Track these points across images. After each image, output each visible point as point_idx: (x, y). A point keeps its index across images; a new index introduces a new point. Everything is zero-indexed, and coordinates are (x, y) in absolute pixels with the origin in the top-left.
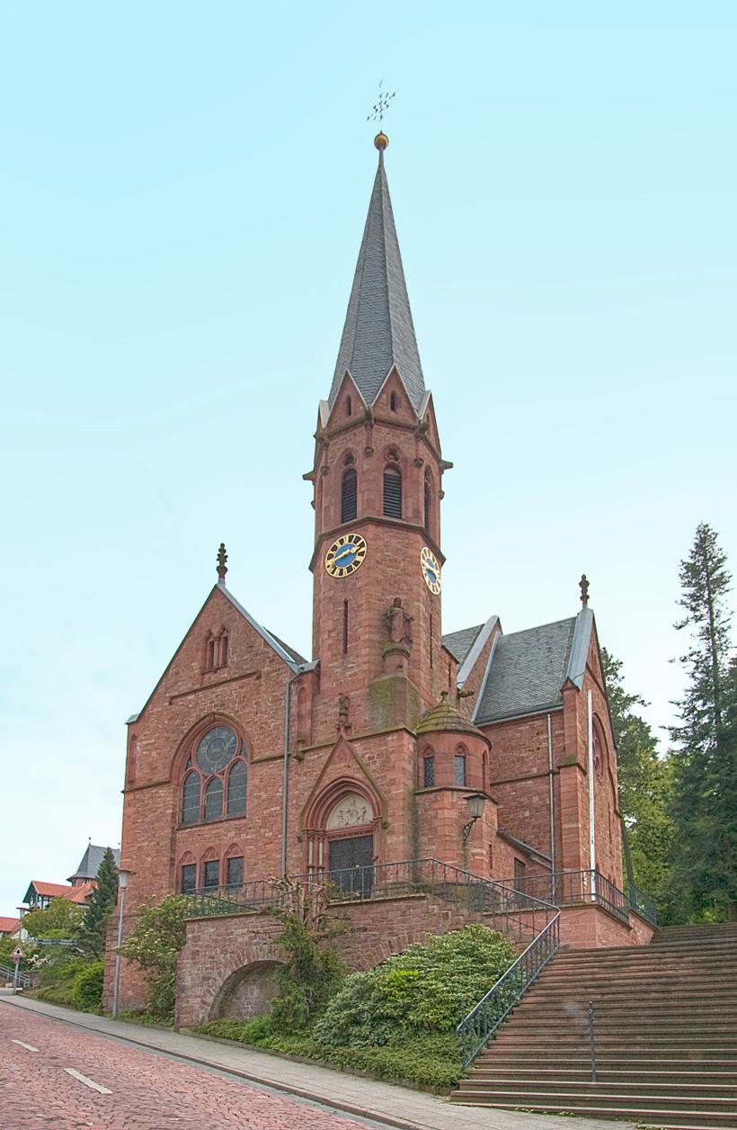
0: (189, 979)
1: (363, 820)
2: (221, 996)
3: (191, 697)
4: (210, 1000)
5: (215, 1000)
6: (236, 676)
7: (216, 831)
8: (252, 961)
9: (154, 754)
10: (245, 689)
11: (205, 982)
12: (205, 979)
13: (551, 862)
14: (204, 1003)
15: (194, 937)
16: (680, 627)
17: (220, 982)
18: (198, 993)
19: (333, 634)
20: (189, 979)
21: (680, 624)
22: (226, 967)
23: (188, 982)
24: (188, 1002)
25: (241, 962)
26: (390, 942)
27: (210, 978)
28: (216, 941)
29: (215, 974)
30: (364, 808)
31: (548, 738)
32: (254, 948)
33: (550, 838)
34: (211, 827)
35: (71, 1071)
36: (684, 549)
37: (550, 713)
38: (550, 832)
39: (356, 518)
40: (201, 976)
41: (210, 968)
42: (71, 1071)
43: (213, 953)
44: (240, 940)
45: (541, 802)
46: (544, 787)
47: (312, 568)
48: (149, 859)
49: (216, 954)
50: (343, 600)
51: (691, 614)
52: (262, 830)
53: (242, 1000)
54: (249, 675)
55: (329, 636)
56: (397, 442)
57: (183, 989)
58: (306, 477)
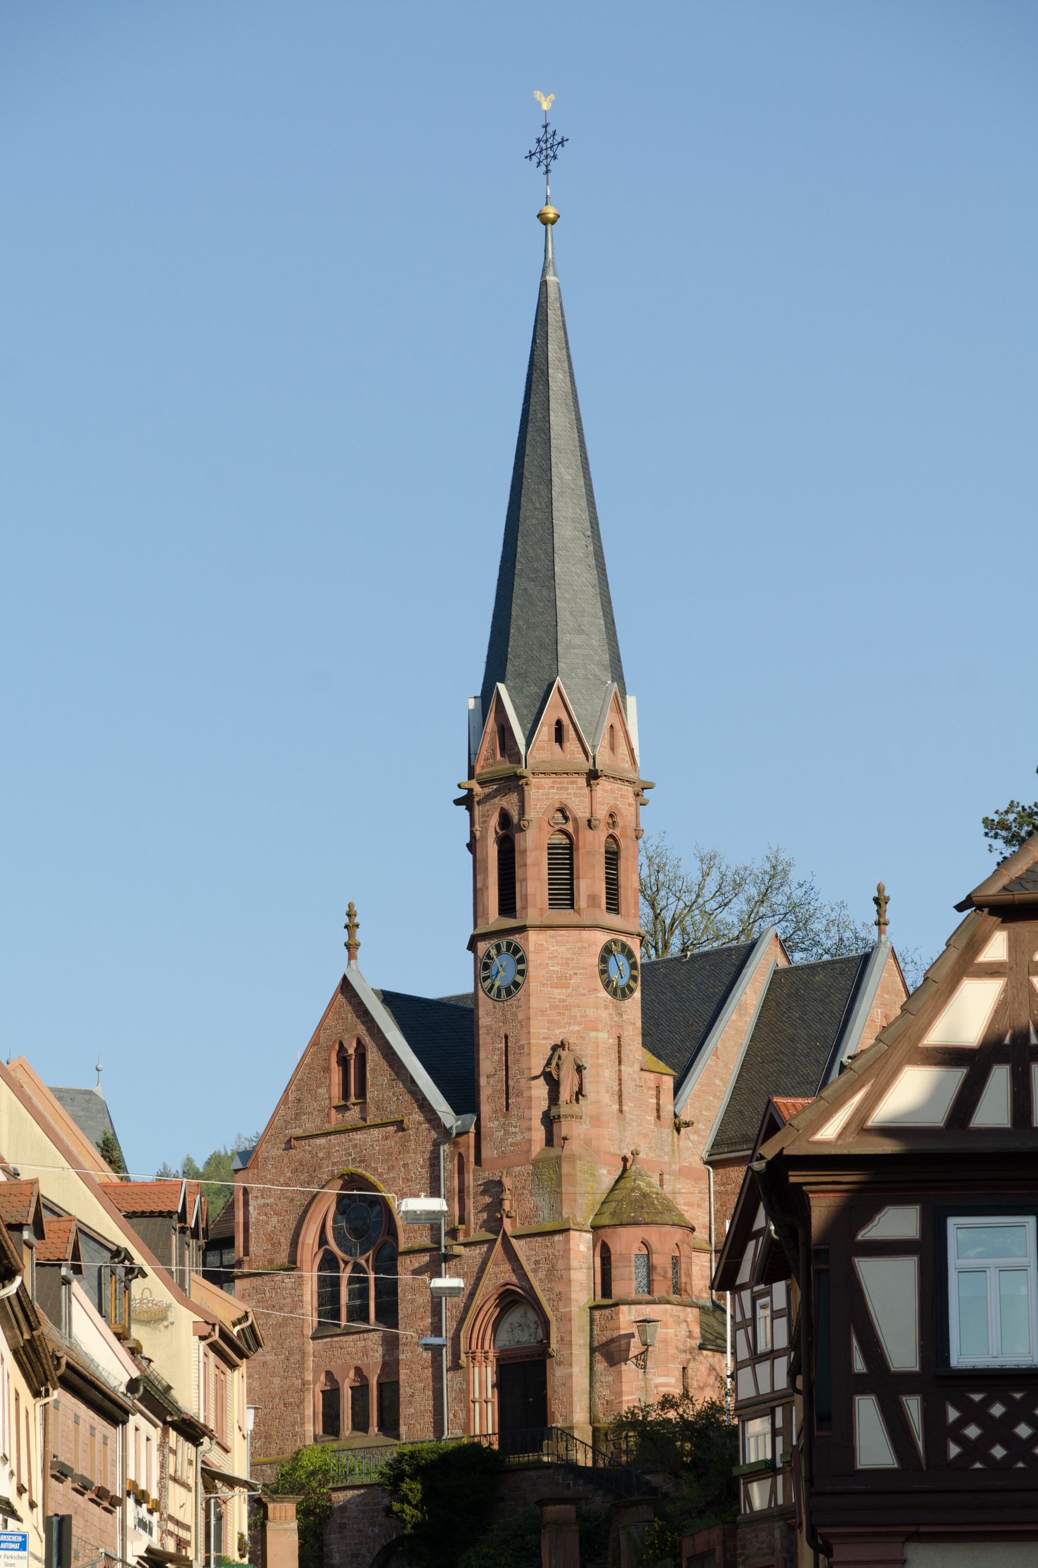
0: (337, 1556)
3: (322, 1141)
9: (274, 1220)
12: (355, 1556)
48: (277, 1381)
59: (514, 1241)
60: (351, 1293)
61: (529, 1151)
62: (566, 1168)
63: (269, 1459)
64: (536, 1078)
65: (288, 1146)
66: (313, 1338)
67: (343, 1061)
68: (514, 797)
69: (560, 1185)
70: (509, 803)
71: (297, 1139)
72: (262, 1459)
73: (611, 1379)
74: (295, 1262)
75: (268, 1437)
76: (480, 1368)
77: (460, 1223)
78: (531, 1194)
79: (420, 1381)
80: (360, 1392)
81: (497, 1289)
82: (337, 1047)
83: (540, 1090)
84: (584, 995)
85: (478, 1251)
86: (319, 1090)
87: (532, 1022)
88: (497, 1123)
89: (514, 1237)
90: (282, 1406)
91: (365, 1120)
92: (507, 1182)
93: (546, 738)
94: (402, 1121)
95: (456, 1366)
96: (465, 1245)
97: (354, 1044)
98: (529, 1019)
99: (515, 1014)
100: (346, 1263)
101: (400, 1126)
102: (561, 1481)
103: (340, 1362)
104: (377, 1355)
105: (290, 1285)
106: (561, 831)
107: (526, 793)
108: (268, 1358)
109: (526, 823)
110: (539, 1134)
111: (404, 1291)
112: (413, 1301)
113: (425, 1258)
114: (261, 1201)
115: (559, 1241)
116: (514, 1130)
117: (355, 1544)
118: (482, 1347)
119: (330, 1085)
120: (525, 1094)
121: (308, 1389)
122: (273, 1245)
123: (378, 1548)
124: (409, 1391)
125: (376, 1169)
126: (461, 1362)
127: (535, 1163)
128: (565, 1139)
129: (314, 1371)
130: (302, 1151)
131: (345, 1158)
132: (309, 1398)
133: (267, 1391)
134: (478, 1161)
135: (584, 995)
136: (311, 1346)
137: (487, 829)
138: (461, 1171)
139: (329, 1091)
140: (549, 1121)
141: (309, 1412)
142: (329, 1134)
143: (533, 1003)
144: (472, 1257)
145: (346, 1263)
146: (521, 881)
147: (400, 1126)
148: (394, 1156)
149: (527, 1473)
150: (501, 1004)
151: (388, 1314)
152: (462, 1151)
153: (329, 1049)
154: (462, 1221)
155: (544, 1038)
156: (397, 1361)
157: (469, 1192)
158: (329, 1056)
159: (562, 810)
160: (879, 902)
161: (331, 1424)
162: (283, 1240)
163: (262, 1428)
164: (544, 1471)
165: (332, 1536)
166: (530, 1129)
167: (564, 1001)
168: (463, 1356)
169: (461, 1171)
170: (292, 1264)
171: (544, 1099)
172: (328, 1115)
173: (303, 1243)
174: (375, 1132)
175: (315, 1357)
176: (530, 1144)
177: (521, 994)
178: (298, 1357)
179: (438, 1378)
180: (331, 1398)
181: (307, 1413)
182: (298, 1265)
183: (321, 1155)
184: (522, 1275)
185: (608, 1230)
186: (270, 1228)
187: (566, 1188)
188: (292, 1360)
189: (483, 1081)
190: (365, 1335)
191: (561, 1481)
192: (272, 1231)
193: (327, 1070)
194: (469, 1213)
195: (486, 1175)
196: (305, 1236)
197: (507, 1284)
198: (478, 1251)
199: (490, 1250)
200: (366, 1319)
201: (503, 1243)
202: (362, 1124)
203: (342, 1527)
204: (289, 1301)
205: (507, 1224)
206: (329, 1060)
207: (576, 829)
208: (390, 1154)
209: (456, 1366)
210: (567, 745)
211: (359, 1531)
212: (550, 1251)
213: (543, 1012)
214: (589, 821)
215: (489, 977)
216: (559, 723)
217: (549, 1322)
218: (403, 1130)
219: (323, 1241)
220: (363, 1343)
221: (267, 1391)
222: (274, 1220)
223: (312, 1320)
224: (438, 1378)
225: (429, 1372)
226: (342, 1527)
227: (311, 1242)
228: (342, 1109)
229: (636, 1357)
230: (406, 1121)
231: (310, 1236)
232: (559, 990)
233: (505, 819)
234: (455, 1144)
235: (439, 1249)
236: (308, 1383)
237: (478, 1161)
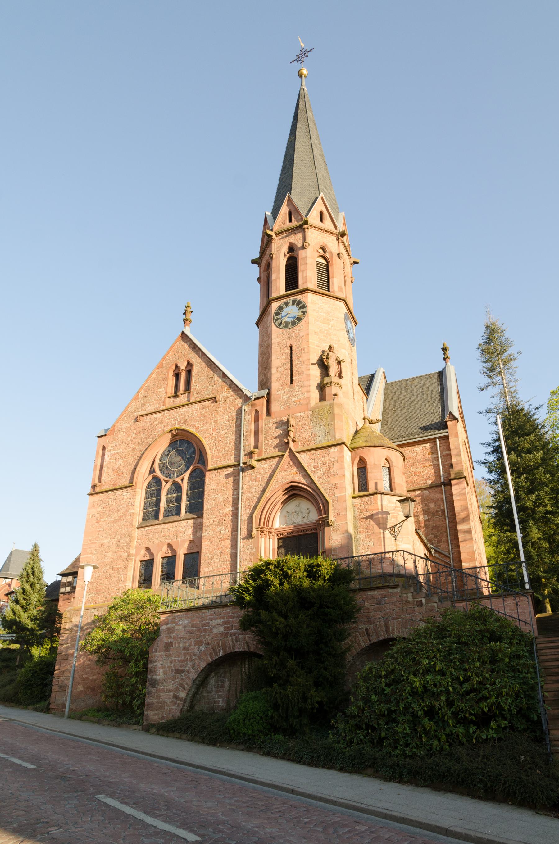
0: (161, 672)
1: (308, 519)
2: (193, 690)
3: (158, 415)
4: (182, 694)
5: (188, 694)
6: (198, 400)
7: (174, 529)
8: (228, 652)
9: (121, 461)
10: (204, 410)
11: (178, 675)
12: (178, 672)
13: (449, 558)
14: (176, 697)
15: (168, 629)
16: (483, 390)
17: (193, 675)
18: (170, 687)
19: (280, 370)
20: (161, 672)
21: (483, 387)
22: (200, 659)
23: (160, 675)
24: (159, 697)
25: (216, 655)
26: (367, 630)
27: (182, 671)
28: (191, 632)
29: (189, 667)
30: (308, 509)
31: (438, 457)
32: (230, 638)
33: (447, 537)
34: (170, 525)
35: (102, 798)
36: (479, 337)
37: (438, 438)
38: (446, 532)
39: (297, 288)
40: (174, 669)
41: (184, 661)
42: (102, 798)
43: (187, 645)
44: (215, 630)
45: (436, 508)
46: (438, 496)
47: (257, 324)
48: (109, 555)
49: (190, 645)
50: (289, 345)
51: (490, 381)
52: (219, 528)
53: (213, 693)
54: (208, 400)
55: (277, 371)
56: (325, 241)
57: (154, 683)
58: (254, 262)
59: (297, 455)
60: (168, 501)
61: (308, 403)
62: (336, 410)
63: (97, 605)
64: (313, 364)
65: (137, 420)
66: (137, 528)
67: (177, 376)
68: (300, 235)
69: (333, 419)
70: (296, 240)
71: (141, 416)
72: (92, 605)
73: (371, 543)
74: (132, 483)
75: (98, 591)
76: (265, 538)
77: (255, 448)
78: (310, 427)
79: (218, 549)
80: (170, 561)
81: (282, 486)
82: (174, 367)
83: (316, 372)
84: (338, 330)
85: (268, 464)
86: (160, 390)
87: (310, 336)
88: (283, 392)
89: (298, 452)
90: (111, 571)
91: (189, 401)
92: (292, 422)
93: (316, 215)
94: (216, 397)
95: (250, 536)
96: (257, 461)
97: (185, 364)
98: (308, 334)
99: (298, 334)
100: (167, 482)
101: (214, 400)
102: (410, 599)
103: (156, 541)
104: (189, 534)
105: (126, 497)
106: (322, 256)
107: (306, 232)
108: (105, 541)
109: (307, 244)
110: (315, 394)
111: (209, 493)
112: (215, 499)
113: (231, 470)
114: (112, 452)
115: (334, 452)
116: (296, 393)
117: (180, 661)
118: (268, 525)
119: (167, 387)
120: (305, 373)
121: (131, 559)
122: (118, 475)
123: (203, 665)
124: (209, 556)
125: (194, 425)
126: (253, 533)
127: (313, 410)
128: (335, 395)
129: (137, 548)
130: (145, 422)
131: (173, 422)
132: (131, 565)
133: (102, 561)
134: (268, 413)
135: (338, 330)
136: (136, 532)
137: (280, 254)
138: (257, 420)
139: (166, 389)
140: (322, 387)
141: (130, 574)
142: (164, 410)
143: (311, 327)
144: (263, 468)
145: (167, 482)
146: (303, 271)
147: (214, 400)
148: (208, 417)
149: (370, 593)
150: (288, 330)
151: (196, 508)
152: (258, 408)
153: (168, 369)
154: (256, 447)
155: (317, 346)
156: (201, 538)
157: (262, 431)
158: (168, 372)
159: (323, 248)
160: (444, 349)
161: (146, 581)
162: (125, 471)
163: (95, 585)
164: (390, 591)
165: (157, 654)
166: (309, 391)
167: (327, 330)
168: (254, 531)
169: (257, 420)
170: (131, 485)
171: (317, 377)
172: (164, 402)
173: (139, 472)
174: (195, 406)
175: (138, 539)
176: (309, 400)
177: (302, 323)
178: (126, 539)
179: (234, 545)
180: (148, 565)
181: (128, 574)
182: (134, 484)
183: (156, 423)
184: (307, 475)
185: (365, 449)
186: (117, 466)
187: (337, 423)
188: (122, 541)
189: (274, 371)
190: (177, 523)
191: (410, 599)
192: (119, 468)
193: (166, 379)
194: (262, 443)
195: (276, 418)
196: (141, 467)
197: (291, 482)
198: (268, 464)
199: (279, 463)
200: (178, 514)
201: (289, 456)
202: (188, 402)
203: (169, 645)
204: (125, 506)
205: (292, 444)
206: (168, 374)
207: (332, 257)
208: (205, 416)
209: (250, 536)
210: (325, 221)
211: (184, 649)
212: (327, 459)
213: (316, 333)
214: (338, 254)
215: (279, 319)
216: (321, 213)
217: (327, 502)
218: (216, 402)
219: (152, 471)
220: (174, 529)
221: (102, 561)
222: (121, 461)
223: (138, 518)
224: (234, 545)
225: (228, 542)
226: (169, 645)
227: (144, 472)
228: (176, 396)
229: (390, 528)
230: (218, 397)
231: (144, 468)
232: (325, 325)
233: (292, 249)
234: (253, 405)
235: (239, 464)
236: (132, 555)
237: (268, 413)
